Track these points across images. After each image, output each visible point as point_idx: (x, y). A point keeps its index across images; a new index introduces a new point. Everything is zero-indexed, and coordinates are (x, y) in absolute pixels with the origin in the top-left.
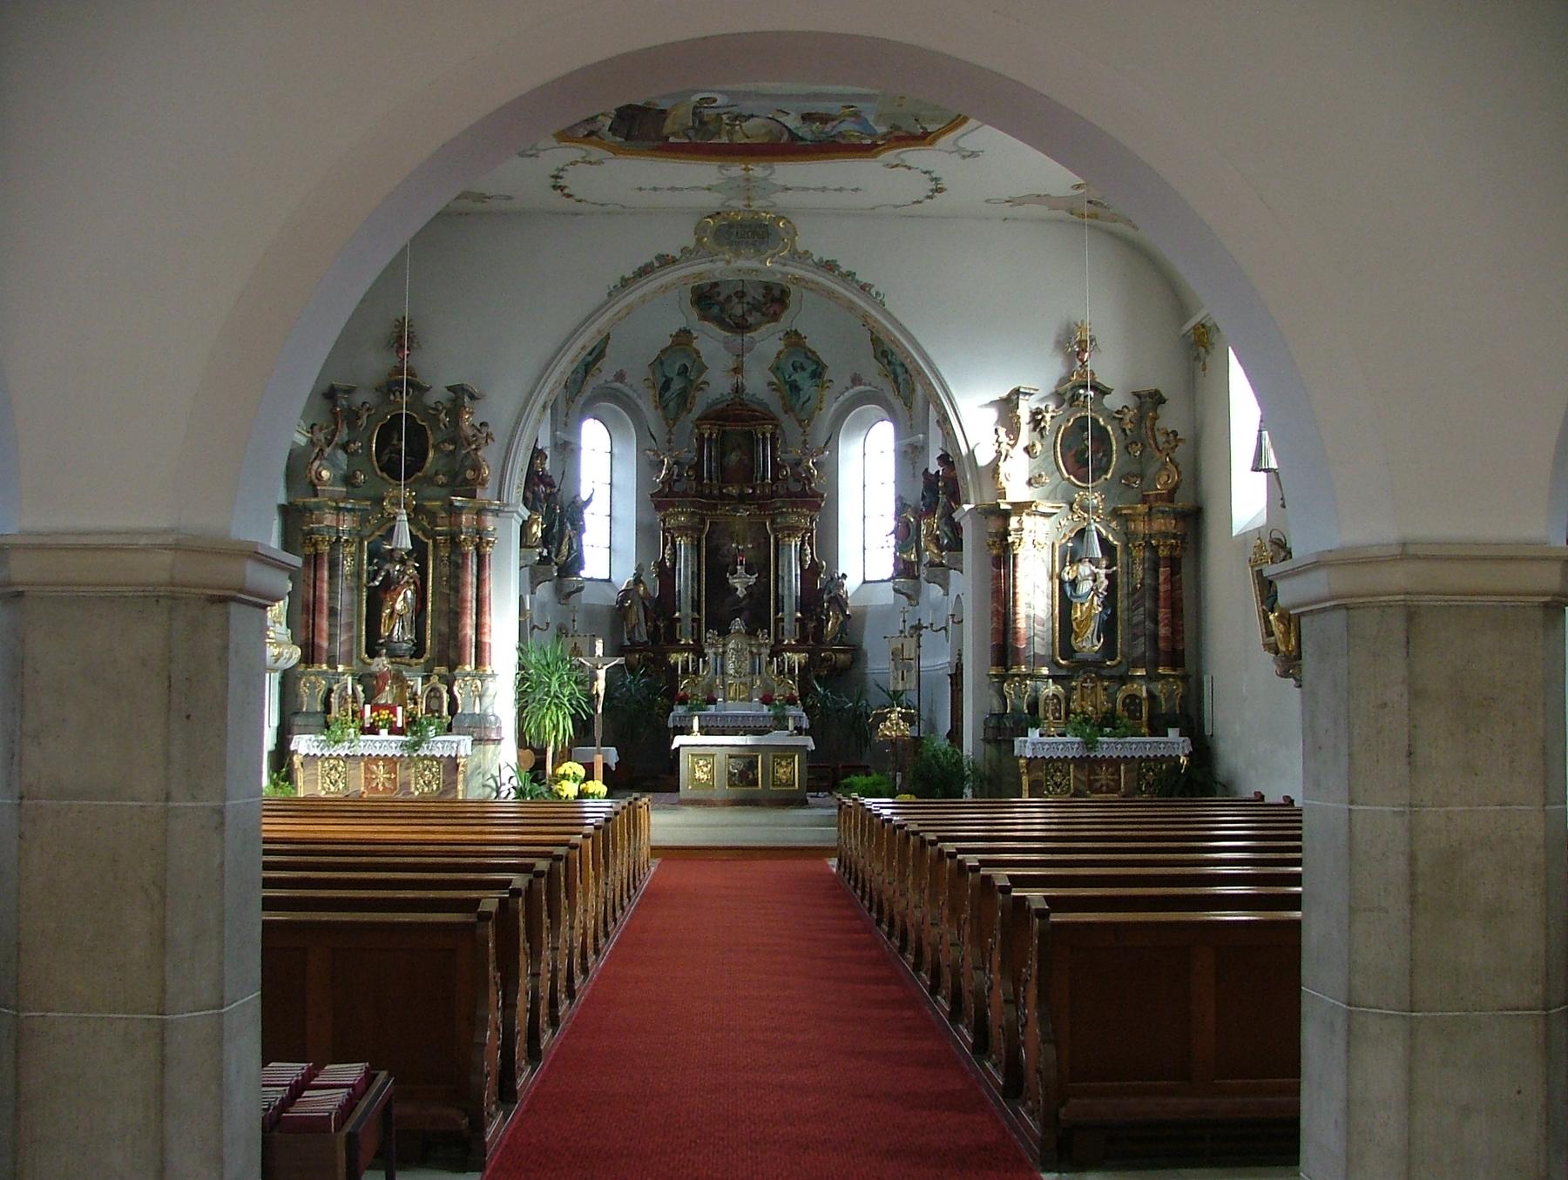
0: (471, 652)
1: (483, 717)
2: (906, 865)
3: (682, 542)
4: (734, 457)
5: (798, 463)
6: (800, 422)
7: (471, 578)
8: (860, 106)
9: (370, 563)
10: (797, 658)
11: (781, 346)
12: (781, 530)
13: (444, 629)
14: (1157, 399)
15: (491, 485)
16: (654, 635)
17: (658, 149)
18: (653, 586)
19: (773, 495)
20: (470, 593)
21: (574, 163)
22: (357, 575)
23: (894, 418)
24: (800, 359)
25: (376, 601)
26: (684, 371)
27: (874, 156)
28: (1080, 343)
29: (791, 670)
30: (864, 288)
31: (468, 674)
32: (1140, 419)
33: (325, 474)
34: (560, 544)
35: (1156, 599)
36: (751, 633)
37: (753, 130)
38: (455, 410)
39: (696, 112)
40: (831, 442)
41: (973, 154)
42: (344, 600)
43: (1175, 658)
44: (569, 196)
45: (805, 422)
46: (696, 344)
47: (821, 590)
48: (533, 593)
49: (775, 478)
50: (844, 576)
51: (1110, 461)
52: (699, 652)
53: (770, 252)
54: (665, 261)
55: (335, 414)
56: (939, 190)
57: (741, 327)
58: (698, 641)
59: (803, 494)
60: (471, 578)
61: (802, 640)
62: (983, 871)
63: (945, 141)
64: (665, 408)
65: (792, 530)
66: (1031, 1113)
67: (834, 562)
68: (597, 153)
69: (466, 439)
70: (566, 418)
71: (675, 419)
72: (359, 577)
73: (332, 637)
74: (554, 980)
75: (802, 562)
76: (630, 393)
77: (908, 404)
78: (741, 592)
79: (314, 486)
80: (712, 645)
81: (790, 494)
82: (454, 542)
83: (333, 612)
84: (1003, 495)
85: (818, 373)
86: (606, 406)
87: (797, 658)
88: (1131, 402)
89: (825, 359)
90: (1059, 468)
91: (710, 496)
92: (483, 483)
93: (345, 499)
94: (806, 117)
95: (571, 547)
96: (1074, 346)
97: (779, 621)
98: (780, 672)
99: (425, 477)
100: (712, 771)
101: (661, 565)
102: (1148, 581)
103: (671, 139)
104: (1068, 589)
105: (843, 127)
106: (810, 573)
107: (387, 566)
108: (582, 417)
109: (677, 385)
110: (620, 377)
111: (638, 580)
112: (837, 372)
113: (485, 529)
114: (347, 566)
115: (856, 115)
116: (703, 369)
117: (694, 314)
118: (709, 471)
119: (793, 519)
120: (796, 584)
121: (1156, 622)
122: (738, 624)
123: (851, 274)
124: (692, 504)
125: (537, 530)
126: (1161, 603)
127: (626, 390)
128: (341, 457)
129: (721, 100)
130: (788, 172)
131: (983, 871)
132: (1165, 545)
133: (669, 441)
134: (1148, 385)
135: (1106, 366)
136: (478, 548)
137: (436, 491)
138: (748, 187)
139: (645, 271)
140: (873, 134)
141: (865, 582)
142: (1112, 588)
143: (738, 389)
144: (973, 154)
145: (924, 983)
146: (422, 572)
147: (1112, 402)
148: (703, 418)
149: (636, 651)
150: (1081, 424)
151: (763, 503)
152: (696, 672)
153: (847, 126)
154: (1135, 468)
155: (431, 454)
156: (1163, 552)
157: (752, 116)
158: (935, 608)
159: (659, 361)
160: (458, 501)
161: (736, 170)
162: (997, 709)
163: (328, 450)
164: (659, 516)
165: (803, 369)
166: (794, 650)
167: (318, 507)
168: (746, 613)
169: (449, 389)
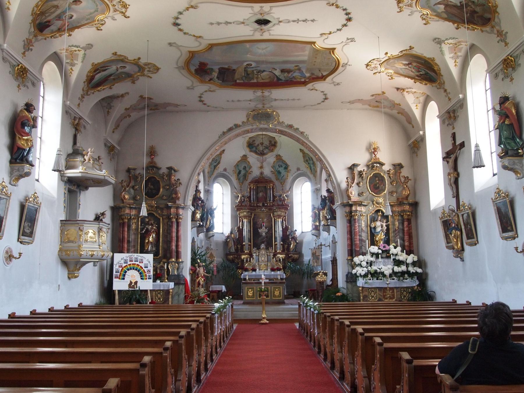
0: (174, 254)
1: (178, 275)
2: (326, 329)
3: (245, 221)
4: (261, 194)
5: (281, 196)
6: (281, 183)
7: (174, 230)
8: (301, 65)
9: (141, 225)
10: (281, 256)
11: (275, 159)
12: (276, 216)
13: (165, 246)
14: (400, 166)
15: (181, 200)
16: (237, 250)
17: (233, 85)
19: (273, 205)
20: (174, 234)
21: (206, 91)
22: (137, 229)
23: (310, 179)
24: (281, 163)
26: (245, 168)
27: (305, 85)
28: (374, 149)
29: (280, 260)
31: (173, 262)
32: (395, 173)
33: (127, 197)
34: (207, 222)
35: (403, 233)
36: (267, 248)
38: (169, 175)
39: (245, 70)
40: (291, 188)
41: (338, 84)
42: (132, 237)
44: (205, 104)
45: (283, 182)
46: (248, 159)
47: (288, 235)
48: (198, 236)
49: (274, 200)
50: (296, 230)
51: (385, 188)
52: (251, 255)
53: (271, 122)
54: (237, 126)
55: (130, 177)
56: (326, 99)
57: (262, 154)
58: (250, 252)
59: (282, 205)
61: (283, 251)
62: (352, 327)
63: (329, 79)
64: (239, 179)
65: (279, 216)
66: (347, 384)
67: (292, 227)
68: (213, 87)
69: (173, 184)
70: (209, 182)
71: (242, 183)
72: (138, 230)
74: (199, 367)
75: (282, 226)
76: (228, 175)
77: (315, 176)
78: (264, 234)
79: (123, 200)
80: (255, 253)
81: (278, 205)
82: (169, 218)
83: (129, 242)
84: (350, 199)
85: (286, 167)
86: (221, 179)
87: (281, 256)
89: (288, 163)
90: (368, 190)
91: (254, 206)
92: (178, 199)
93: (133, 205)
94: (283, 71)
95: (210, 223)
96: (373, 150)
97: (275, 245)
98: (277, 261)
100: (253, 293)
103: (238, 81)
104: (373, 230)
106: (285, 230)
107: (147, 226)
108: (213, 183)
109: (243, 172)
110: (225, 170)
111: (231, 233)
112: (292, 167)
113: (179, 214)
114: (134, 226)
115: (299, 69)
116: (250, 167)
117: (248, 150)
118: (253, 199)
119: (279, 213)
120: (281, 233)
122: (263, 246)
123: (297, 129)
124: (248, 209)
125: (198, 216)
126: (406, 234)
127: (227, 174)
128: (132, 191)
129: (254, 64)
131: (352, 327)
132: (406, 215)
133: (241, 190)
134: (397, 161)
136: (177, 220)
138: (263, 100)
139: (230, 129)
140: (305, 77)
141: (302, 232)
142: (388, 229)
143: (262, 173)
144: (338, 84)
145: (337, 376)
146: (159, 228)
147: (386, 168)
148: (251, 182)
149: (231, 255)
150: (376, 176)
151: (271, 209)
152: (250, 261)
153: (297, 74)
154: (394, 190)
155: (161, 190)
156: (406, 217)
157: (264, 71)
158: (325, 240)
159: (237, 165)
160: (170, 204)
161: (259, 93)
163: (127, 189)
165: (282, 166)
167: (124, 207)
168: (265, 243)
169: (168, 168)
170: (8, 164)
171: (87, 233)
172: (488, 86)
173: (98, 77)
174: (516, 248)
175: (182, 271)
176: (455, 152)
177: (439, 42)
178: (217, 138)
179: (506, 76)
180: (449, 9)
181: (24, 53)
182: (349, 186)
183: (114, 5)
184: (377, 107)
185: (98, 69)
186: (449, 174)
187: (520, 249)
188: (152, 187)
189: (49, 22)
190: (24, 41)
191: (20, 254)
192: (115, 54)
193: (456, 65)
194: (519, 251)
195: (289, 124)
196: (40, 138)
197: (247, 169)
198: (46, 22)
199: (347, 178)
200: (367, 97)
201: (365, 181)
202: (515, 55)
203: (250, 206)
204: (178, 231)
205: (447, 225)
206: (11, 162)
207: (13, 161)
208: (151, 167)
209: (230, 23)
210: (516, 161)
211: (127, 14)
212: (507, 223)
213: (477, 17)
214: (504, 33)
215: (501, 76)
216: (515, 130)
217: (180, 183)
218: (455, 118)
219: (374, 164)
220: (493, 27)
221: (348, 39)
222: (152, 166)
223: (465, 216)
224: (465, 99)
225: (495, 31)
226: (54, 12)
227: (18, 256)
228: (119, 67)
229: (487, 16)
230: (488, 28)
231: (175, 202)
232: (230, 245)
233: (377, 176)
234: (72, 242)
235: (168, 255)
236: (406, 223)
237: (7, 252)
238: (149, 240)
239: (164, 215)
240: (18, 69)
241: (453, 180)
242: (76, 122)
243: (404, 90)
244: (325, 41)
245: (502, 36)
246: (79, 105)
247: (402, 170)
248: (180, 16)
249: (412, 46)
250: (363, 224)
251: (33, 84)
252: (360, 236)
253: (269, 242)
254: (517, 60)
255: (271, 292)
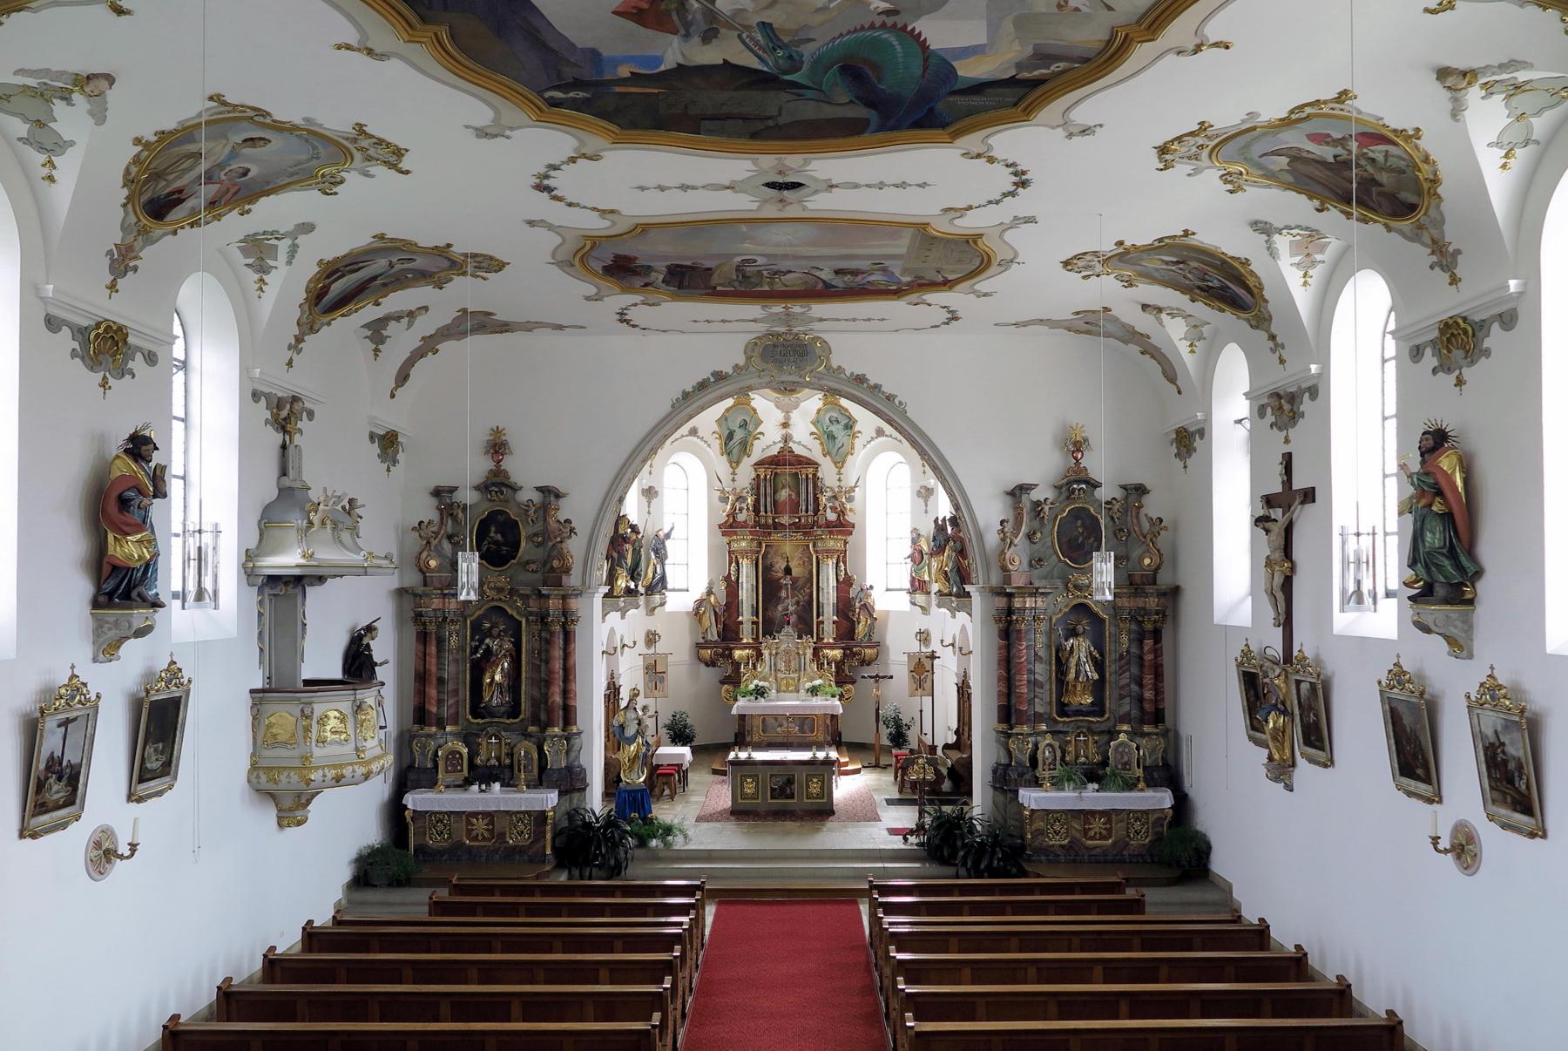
7: (557, 653)
8: (887, 263)
9: (472, 639)
10: (836, 653)
13: (536, 694)
14: (1141, 490)
18: (721, 589)
20: (557, 665)
25: (478, 670)
26: (744, 425)
30: (890, 398)
32: (1126, 510)
33: (433, 563)
35: (1142, 666)
37: (792, 281)
43: (1158, 717)
60: (557, 653)
71: (738, 463)
73: (440, 702)
82: (543, 618)
88: (1119, 494)
91: (766, 526)
92: (567, 571)
94: (837, 272)
99: (519, 563)
101: (727, 578)
102: (1134, 650)
105: (871, 278)
106: (845, 584)
111: (710, 592)
115: (885, 270)
119: (831, 544)
121: (1141, 685)
123: (877, 387)
126: (1146, 670)
129: (760, 261)
130: (819, 309)
135: (1098, 464)
136: (564, 626)
137: (530, 577)
143: (786, 439)
147: (1103, 494)
150: (1078, 514)
155: (523, 544)
156: (1149, 626)
161: (778, 308)
162: (1004, 761)
164: (726, 539)
166: (832, 647)
169: (542, 490)
170: (87, 609)
171: (323, 721)
172: (1391, 409)
173: (337, 288)
174: (1435, 840)
175: (578, 757)
176: (1286, 506)
177: (1263, 228)
178: (667, 408)
179: (1443, 367)
180: (1302, 168)
181: (112, 287)
182: (1006, 540)
183: (362, 149)
184: (1088, 332)
185: (337, 271)
186: (1269, 563)
187: (1444, 843)
188: (499, 537)
189: (180, 191)
190: (110, 253)
191: (133, 847)
192: (382, 237)
193: (1305, 284)
194: (1441, 847)
195: (858, 372)
196: (184, 478)
197: (751, 427)
198: (173, 193)
199: (1002, 522)
200: (1066, 315)
201: (1046, 530)
202: (1477, 318)
203: (757, 524)
204: (567, 655)
205: (1252, 684)
206: (95, 604)
207: (102, 599)
208: (494, 484)
209: (694, 188)
210: (1454, 616)
211: (404, 165)
212: (1415, 756)
213: (1379, 194)
214: (1451, 249)
215: (1430, 360)
216: (1456, 532)
217: (572, 530)
218: (1295, 417)
219: (1076, 482)
220: (1420, 227)
221: (1016, 218)
222: (497, 484)
223: (1305, 687)
224: (1325, 373)
225: (1426, 238)
226: (191, 169)
227: (127, 853)
228: (394, 260)
229: (1410, 198)
230: (1405, 224)
231: (559, 584)
232: (707, 624)
233: (1078, 514)
234: (285, 744)
235: (543, 717)
236: (1148, 643)
237: (98, 845)
238: (493, 679)
239: (531, 614)
240: (97, 336)
241: (1278, 580)
242: (284, 413)
243: (1160, 310)
244: (956, 222)
245: (1445, 259)
246: (290, 364)
247: (1146, 499)
248: (552, 173)
249: (1192, 229)
250: (1041, 640)
251: (151, 358)
252: (1031, 672)
253: (806, 624)
254: (1479, 335)
255: (800, 786)
